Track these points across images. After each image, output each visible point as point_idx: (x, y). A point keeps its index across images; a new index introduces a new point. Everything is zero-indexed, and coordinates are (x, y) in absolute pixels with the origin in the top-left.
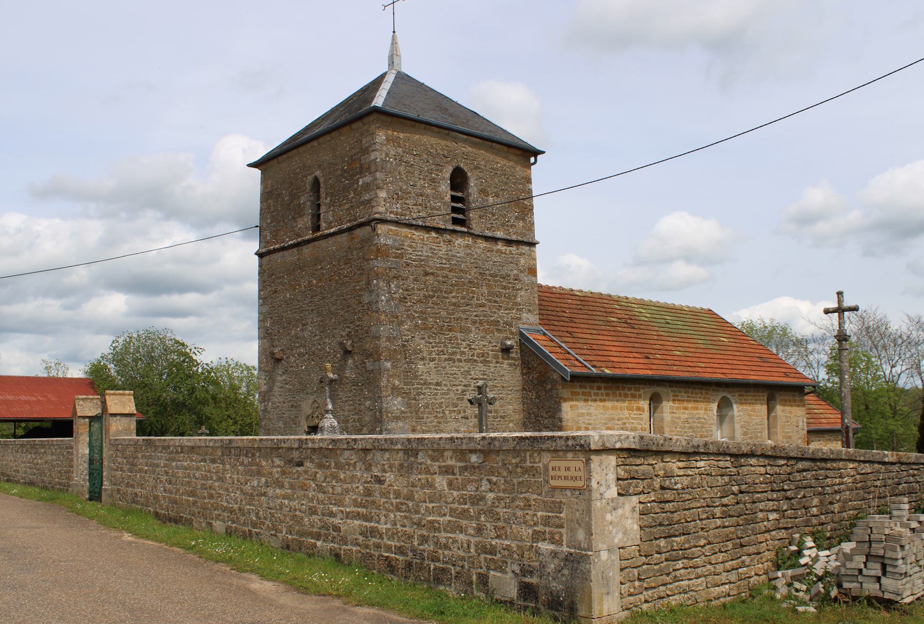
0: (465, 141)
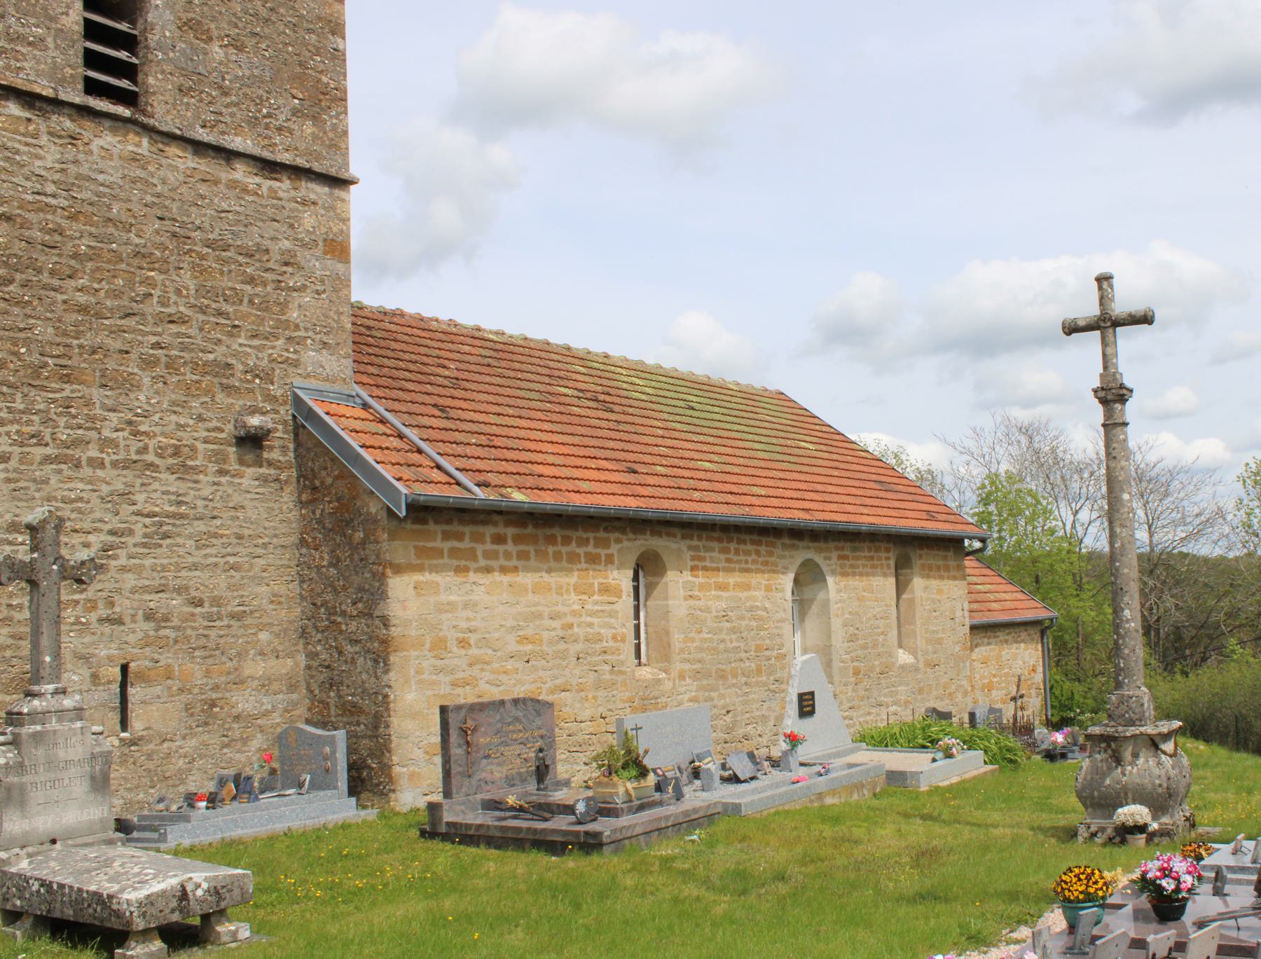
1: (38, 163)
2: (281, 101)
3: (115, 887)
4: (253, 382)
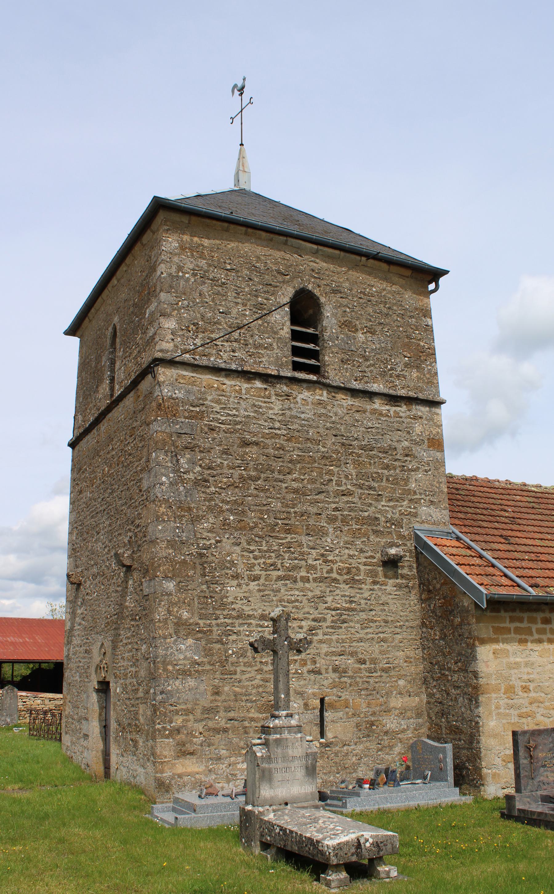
0: (315, 253)
1: (271, 412)
2: (398, 360)
3: (320, 836)
4: (391, 527)
